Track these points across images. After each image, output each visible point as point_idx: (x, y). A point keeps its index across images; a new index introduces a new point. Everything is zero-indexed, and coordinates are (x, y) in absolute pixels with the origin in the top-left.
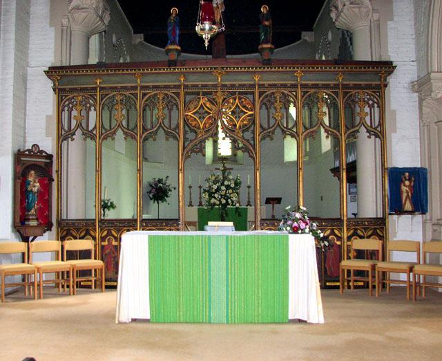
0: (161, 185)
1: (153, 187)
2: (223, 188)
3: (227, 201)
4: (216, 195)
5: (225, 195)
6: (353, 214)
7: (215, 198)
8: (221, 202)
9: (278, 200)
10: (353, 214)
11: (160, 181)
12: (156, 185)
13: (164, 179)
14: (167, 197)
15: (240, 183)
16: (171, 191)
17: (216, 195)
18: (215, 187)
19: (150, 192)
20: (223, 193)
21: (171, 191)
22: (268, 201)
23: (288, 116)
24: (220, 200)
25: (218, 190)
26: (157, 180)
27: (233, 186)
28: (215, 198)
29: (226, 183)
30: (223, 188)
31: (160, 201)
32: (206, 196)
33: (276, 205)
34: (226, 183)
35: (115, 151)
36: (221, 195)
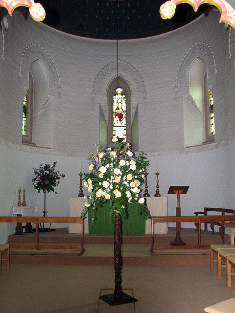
0: (47, 172)
1: (39, 175)
2: (117, 171)
3: (124, 195)
4: (105, 184)
5: (121, 184)
6: (194, 213)
7: (104, 189)
8: (113, 196)
9: (185, 190)
10: (194, 213)
11: (47, 167)
12: (42, 171)
13: (52, 165)
14: (55, 185)
15: (147, 164)
16: (59, 178)
17: (105, 184)
18: (103, 170)
19: (35, 180)
20: (118, 180)
21: (59, 178)
22: (172, 190)
23: (119, 5)
24: (111, 192)
25: (107, 176)
26: (44, 166)
27: (133, 167)
28: (104, 189)
29: (122, 163)
30: (117, 171)
31: (47, 191)
32: (89, 185)
33: (181, 195)
34: (122, 163)
35: (37, 147)
36: (114, 184)
